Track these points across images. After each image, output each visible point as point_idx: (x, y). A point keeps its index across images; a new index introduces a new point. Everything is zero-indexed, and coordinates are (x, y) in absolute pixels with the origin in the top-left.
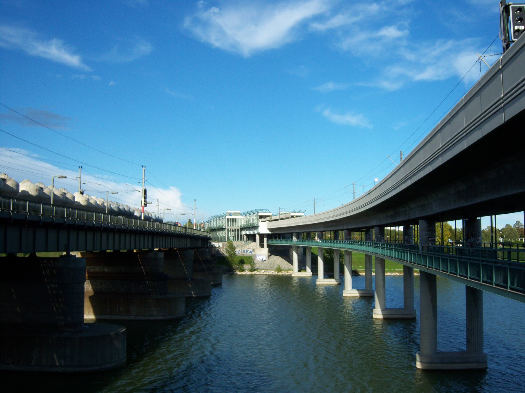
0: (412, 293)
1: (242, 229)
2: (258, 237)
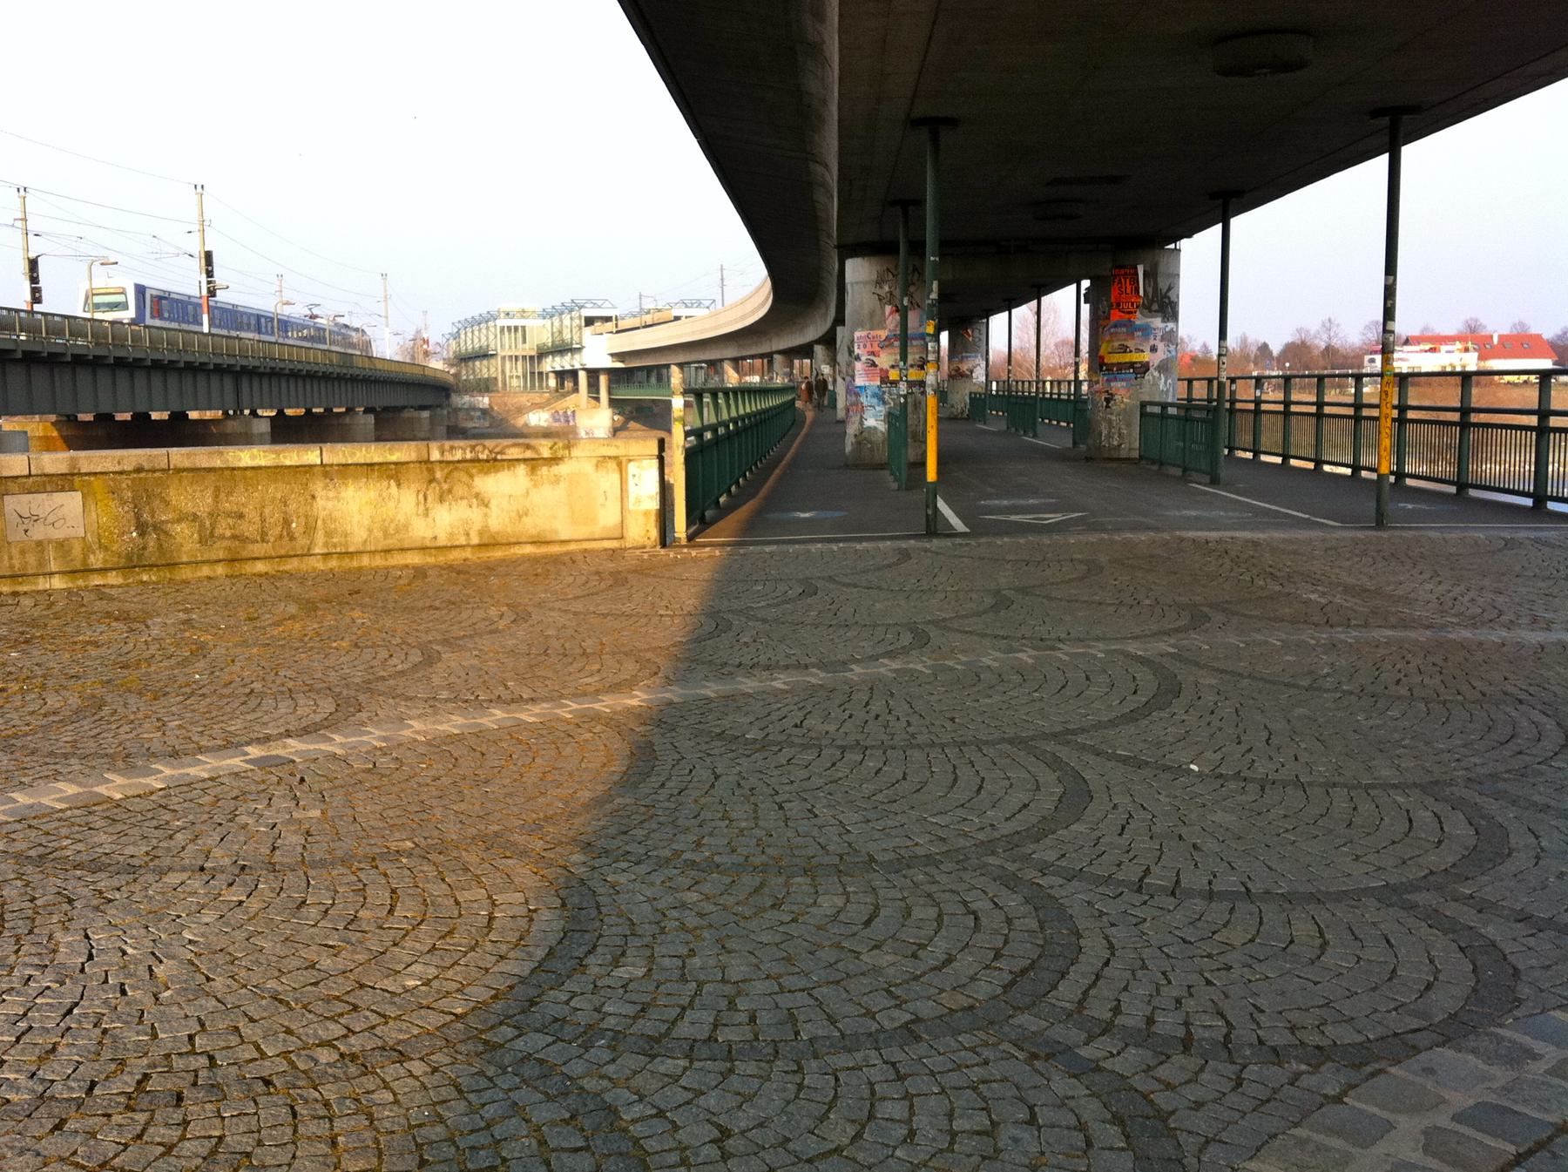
0: (1006, 507)
1: (542, 354)
2: (582, 376)
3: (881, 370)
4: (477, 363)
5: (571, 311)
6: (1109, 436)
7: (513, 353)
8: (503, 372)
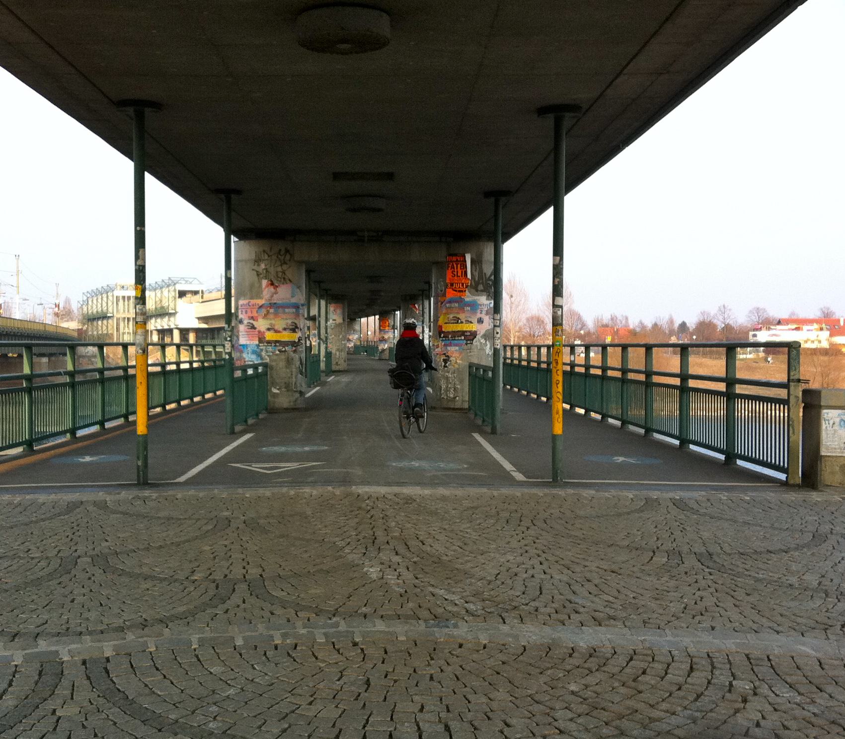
3: (259, 332)
4: (100, 322)
5: (168, 286)
6: (447, 390)
7: (126, 315)
8: (118, 330)
